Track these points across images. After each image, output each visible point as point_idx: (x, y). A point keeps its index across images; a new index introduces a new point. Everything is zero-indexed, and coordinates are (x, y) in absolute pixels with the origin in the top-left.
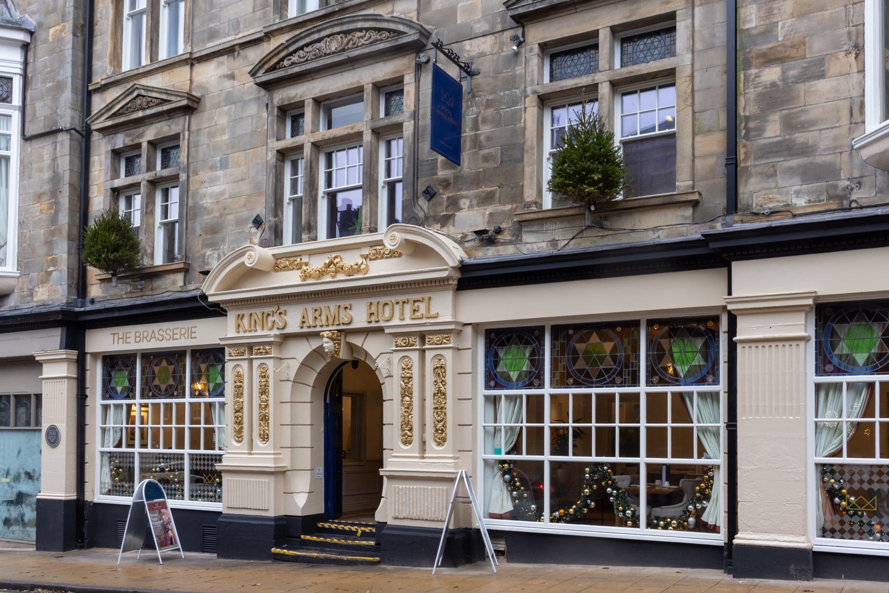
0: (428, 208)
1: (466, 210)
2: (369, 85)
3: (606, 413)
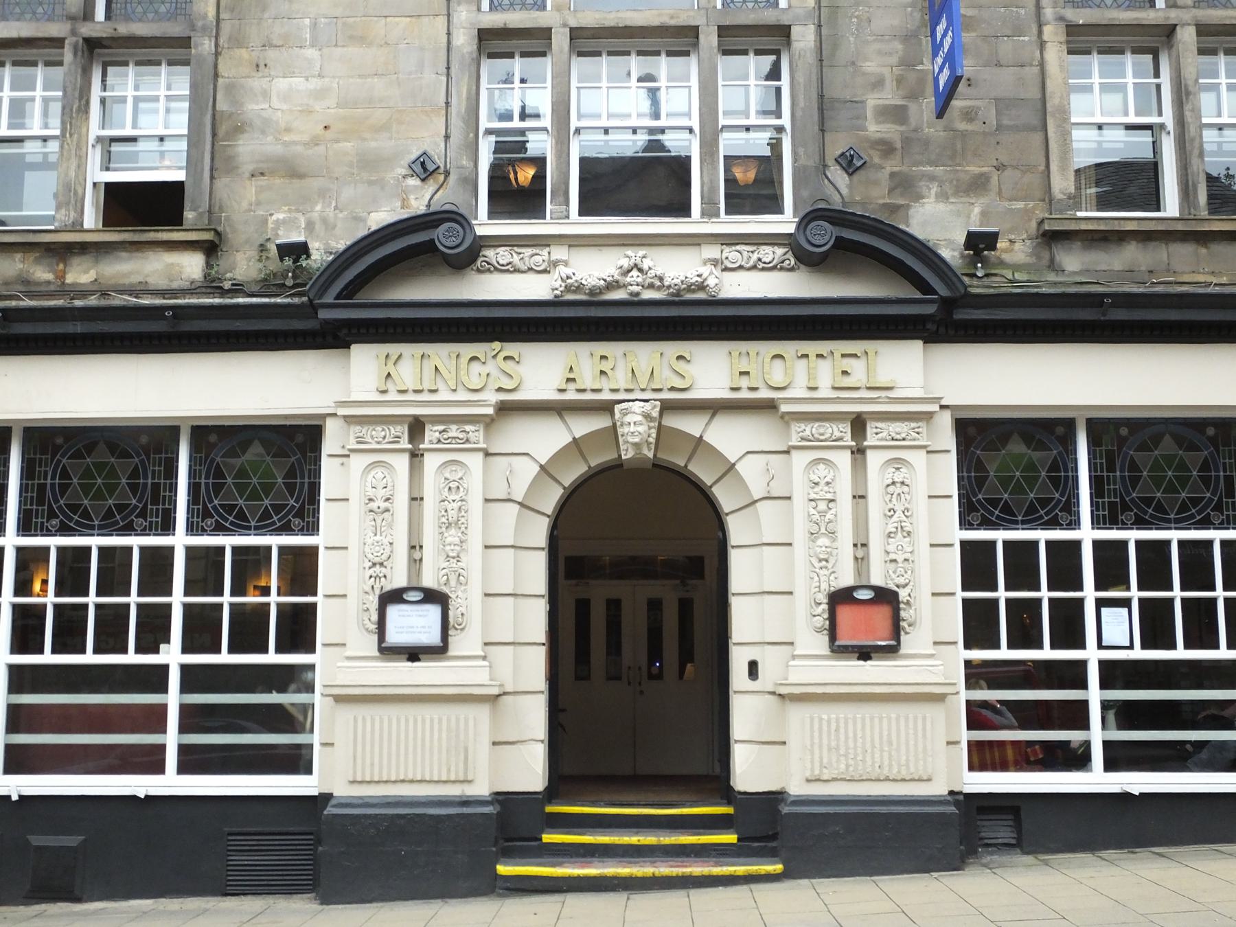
0: (850, 187)
1: (932, 199)
3: (114, 579)
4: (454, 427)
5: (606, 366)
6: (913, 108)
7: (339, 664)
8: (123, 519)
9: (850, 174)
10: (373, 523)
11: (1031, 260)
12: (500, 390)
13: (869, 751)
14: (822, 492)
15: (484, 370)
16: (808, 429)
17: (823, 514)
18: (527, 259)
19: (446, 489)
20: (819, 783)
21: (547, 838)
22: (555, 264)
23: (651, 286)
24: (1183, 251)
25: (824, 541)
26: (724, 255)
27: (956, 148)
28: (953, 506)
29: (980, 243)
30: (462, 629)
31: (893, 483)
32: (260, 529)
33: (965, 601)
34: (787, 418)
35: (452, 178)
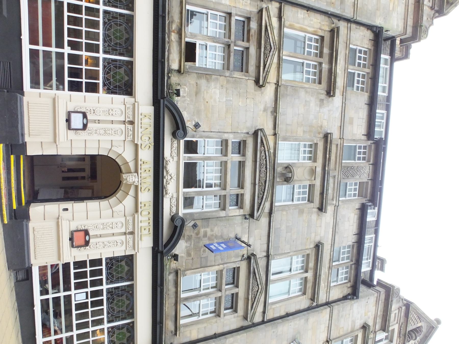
0: (189, 226)
1: (186, 245)
2: (243, 191)
4: (132, 133)
5: (147, 171)
6: (206, 239)
7: (65, 100)
8: (107, 40)
9: (192, 226)
10: (106, 111)
11: (171, 268)
12: (141, 145)
13: (43, 243)
14: (114, 225)
15: (147, 141)
16: (131, 221)
17: (109, 226)
18: (174, 151)
19: (115, 130)
20: (33, 231)
21: (12, 157)
22: (173, 158)
23: (167, 181)
24: (173, 301)
25: (102, 227)
26: (174, 199)
27: (197, 249)
28: (111, 255)
29: (176, 257)
30: (75, 134)
31: (117, 243)
32: (104, 78)
33: (86, 261)
34: (133, 215)
35: (194, 133)
